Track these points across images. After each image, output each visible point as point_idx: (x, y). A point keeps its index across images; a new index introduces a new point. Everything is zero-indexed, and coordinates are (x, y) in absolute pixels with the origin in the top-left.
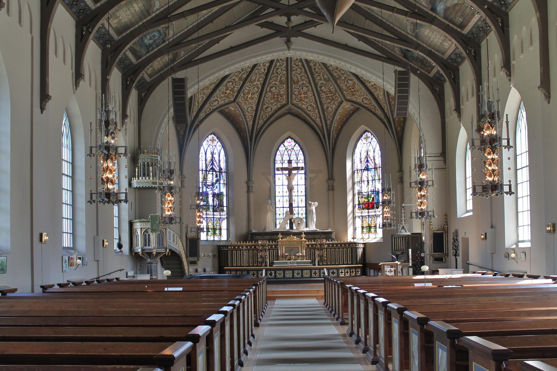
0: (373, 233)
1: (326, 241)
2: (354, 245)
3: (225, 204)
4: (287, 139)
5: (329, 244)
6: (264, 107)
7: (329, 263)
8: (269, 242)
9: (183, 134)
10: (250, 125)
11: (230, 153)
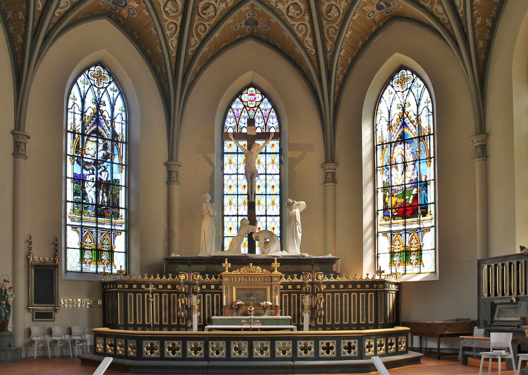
0: (414, 263)
1: (324, 277)
2: (381, 286)
3: (122, 204)
4: (248, 87)
5: (329, 284)
7: (329, 321)
8: (204, 278)
9: (22, 42)
10: (173, 46)
11: (135, 107)
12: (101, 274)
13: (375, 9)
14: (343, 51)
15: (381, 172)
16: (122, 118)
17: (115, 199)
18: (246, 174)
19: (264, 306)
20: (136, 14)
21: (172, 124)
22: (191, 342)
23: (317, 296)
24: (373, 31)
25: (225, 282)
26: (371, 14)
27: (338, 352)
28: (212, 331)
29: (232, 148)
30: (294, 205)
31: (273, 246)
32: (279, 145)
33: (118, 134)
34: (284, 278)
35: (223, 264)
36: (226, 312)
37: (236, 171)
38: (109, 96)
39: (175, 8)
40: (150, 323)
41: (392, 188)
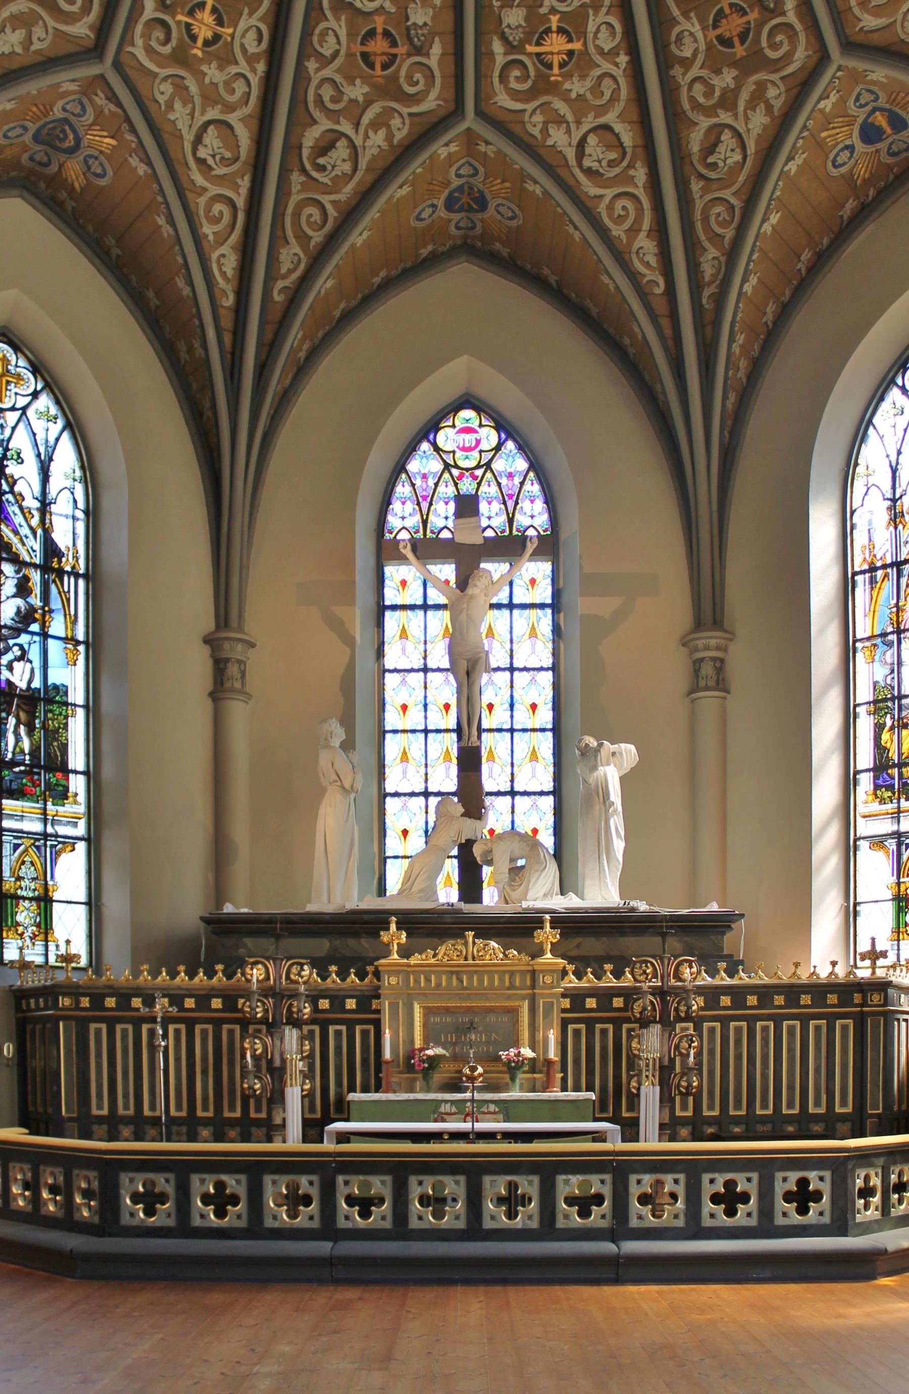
1: (699, 972)
2: (876, 998)
5: (712, 994)
6: (310, 138)
7: (711, 1107)
8: (324, 976)
10: (224, 274)
12: (12, 967)
13: (856, 140)
14: (753, 280)
15: (868, 653)
16: (75, 501)
17: (55, 744)
18: (453, 669)
19: (509, 1061)
20: (110, 173)
21: (225, 517)
22: (276, 1177)
23: (674, 1030)
24: (845, 217)
25: (387, 989)
26: (844, 156)
27: (766, 1210)
28: (348, 1141)
29: (410, 592)
30: (604, 753)
31: (538, 879)
32: (553, 580)
33: (63, 549)
34: (572, 977)
35: (382, 933)
37: (422, 661)
38: (34, 435)
39: (227, 150)
40: (157, 1113)
41: (904, 701)
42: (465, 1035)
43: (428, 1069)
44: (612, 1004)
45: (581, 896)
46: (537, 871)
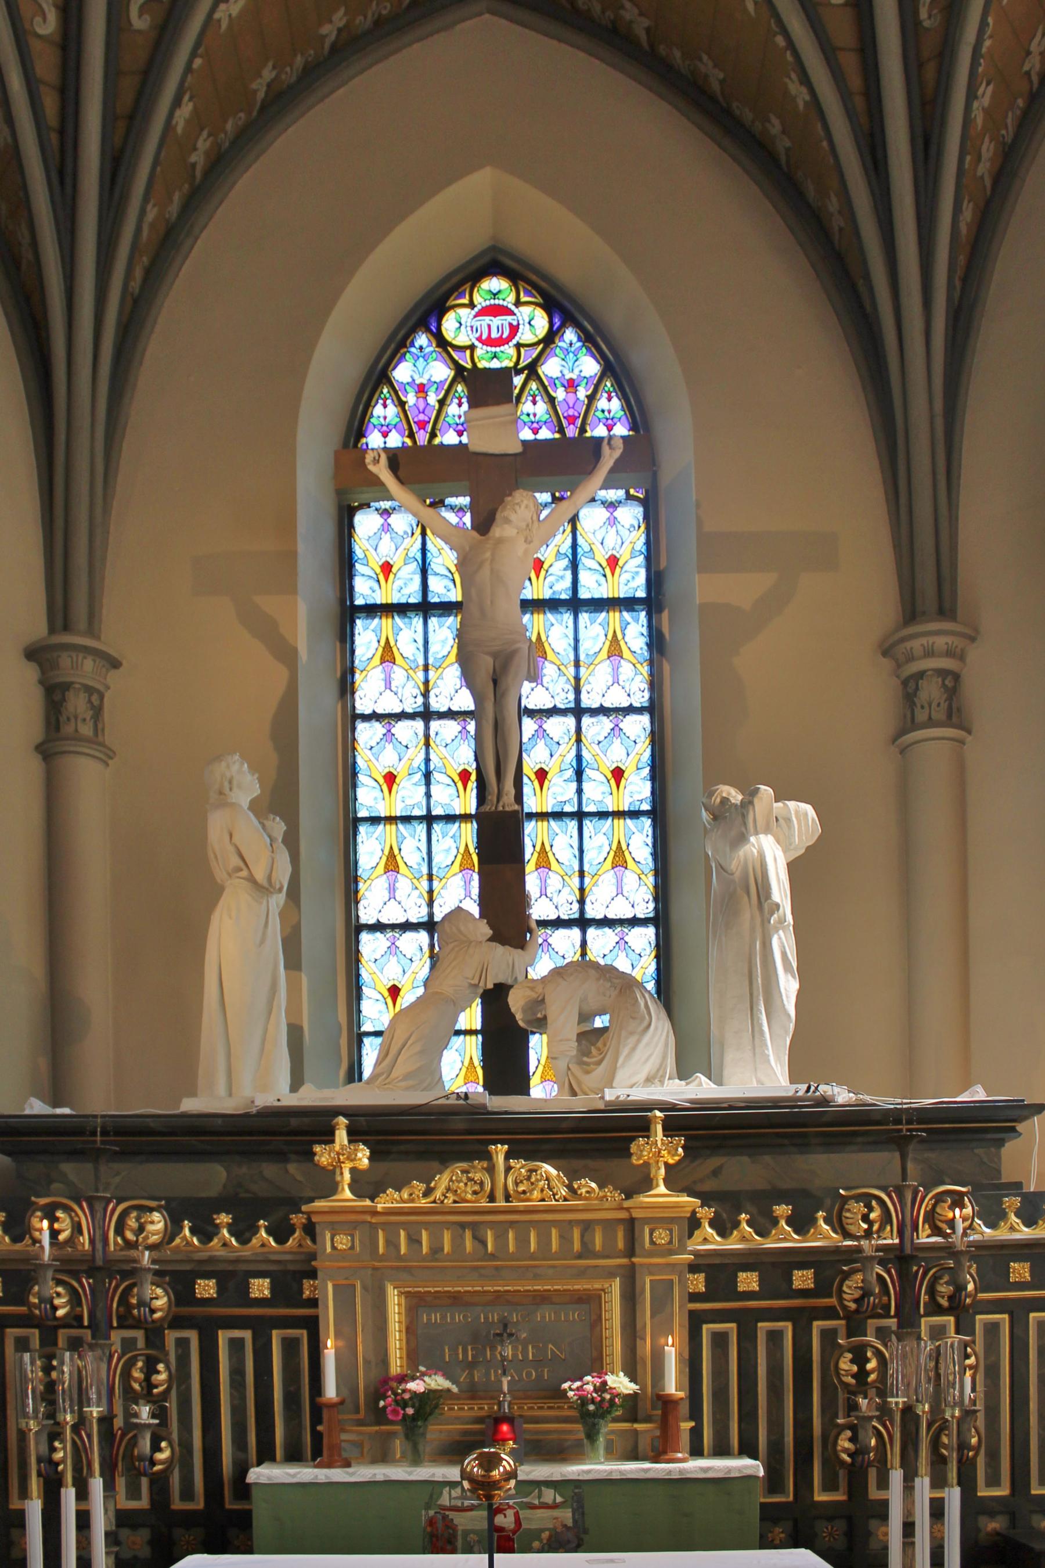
4: (474, 274)
8: (206, 1231)
19: (584, 1401)
29: (398, 583)
31: (634, 1049)
32: (648, 559)
35: (317, 1149)
36: (344, 1436)
37: (420, 700)
42: (493, 1348)
43: (414, 1418)
44: (791, 1282)
45: (719, 1082)
46: (632, 1033)
